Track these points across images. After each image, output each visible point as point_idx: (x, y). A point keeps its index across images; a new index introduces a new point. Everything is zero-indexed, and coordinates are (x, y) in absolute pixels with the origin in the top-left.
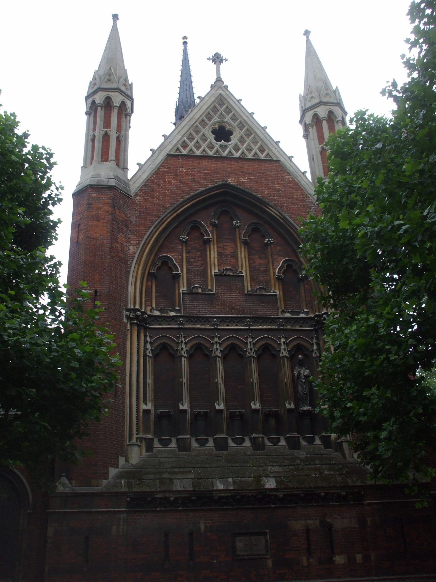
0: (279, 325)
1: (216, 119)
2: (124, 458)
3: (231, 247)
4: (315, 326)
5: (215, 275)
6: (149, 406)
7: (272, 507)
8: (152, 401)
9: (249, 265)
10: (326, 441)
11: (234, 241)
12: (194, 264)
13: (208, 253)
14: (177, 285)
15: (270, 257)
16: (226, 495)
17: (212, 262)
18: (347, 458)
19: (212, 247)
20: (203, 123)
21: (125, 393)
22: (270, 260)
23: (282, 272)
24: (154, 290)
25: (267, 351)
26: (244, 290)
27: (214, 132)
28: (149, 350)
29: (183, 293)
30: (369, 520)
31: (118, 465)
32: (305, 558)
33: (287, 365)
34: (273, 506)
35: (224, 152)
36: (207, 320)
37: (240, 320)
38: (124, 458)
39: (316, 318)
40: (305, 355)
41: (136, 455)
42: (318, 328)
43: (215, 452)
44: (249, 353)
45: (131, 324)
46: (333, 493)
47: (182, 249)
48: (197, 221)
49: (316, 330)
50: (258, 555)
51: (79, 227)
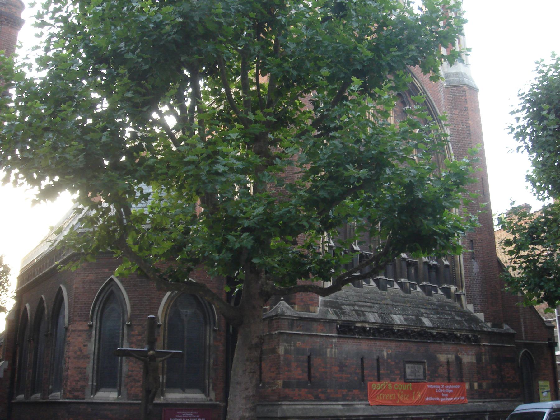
7: (428, 342)
10: (447, 292)
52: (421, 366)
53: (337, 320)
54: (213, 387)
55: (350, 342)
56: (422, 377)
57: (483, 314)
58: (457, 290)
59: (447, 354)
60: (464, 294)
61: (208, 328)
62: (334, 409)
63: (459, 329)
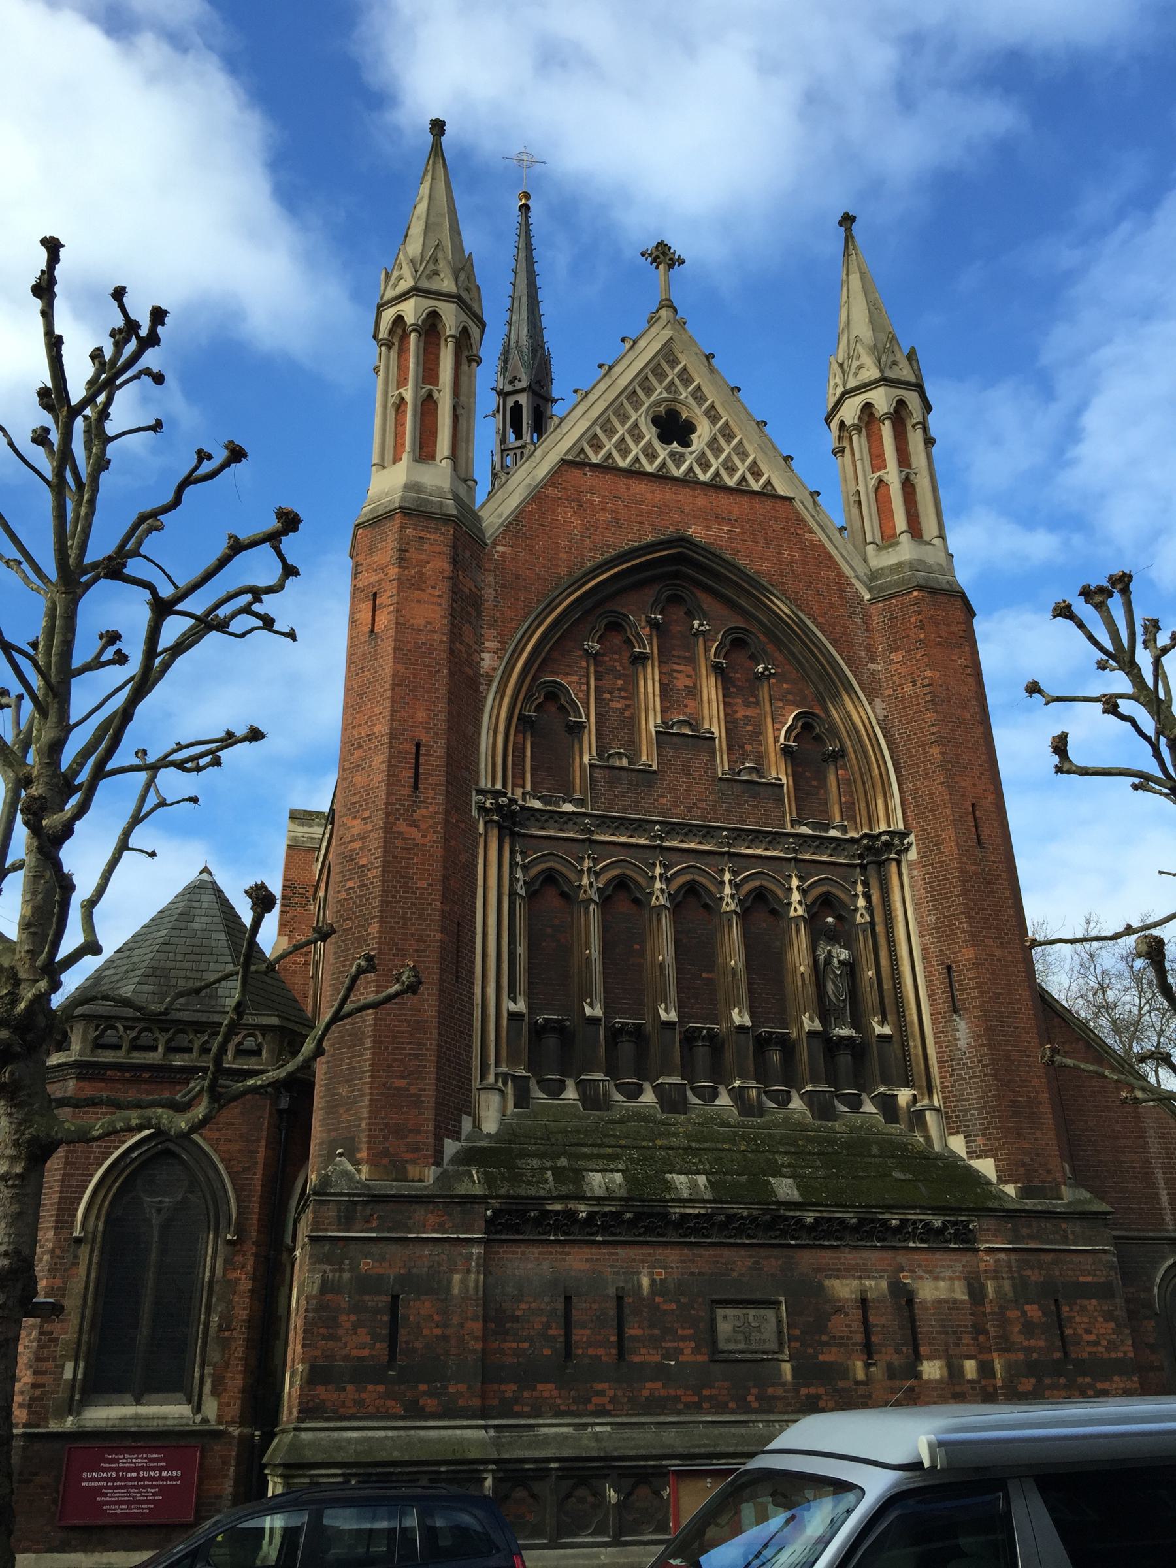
0: (787, 850)
1: (661, 393)
2: (471, 1118)
3: (688, 676)
4: (861, 857)
5: (657, 732)
6: (521, 1006)
9: (726, 715)
11: (692, 661)
12: (612, 704)
13: (642, 683)
14: (577, 747)
15: (767, 704)
16: (697, 1211)
17: (651, 706)
20: (632, 397)
21: (474, 973)
22: (768, 709)
23: (792, 739)
24: (528, 753)
26: (715, 769)
27: (656, 421)
28: (521, 883)
29: (591, 765)
30: (990, 1285)
32: (859, 1364)
34: (793, 1242)
35: (678, 468)
38: (471, 1118)
39: (865, 842)
40: (839, 918)
42: (868, 863)
43: (661, 1116)
44: (727, 904)
45: (486, 823)
46: (915, 1222)
47: (588, 669)
48: (616, 612)
49: (863, 867)
50: (764, 1353)
51: (374, 600)
52: (770, 1314)
53: (485, 1197)
54: (213, 1386)
55: (534, 1252)
56: (773, 1346)
57: (991, 1161)
58: (915, 1100)
59: (860, 1278)
60: (938, 1110)
61: (211, 1236)
62: (461, 1441)
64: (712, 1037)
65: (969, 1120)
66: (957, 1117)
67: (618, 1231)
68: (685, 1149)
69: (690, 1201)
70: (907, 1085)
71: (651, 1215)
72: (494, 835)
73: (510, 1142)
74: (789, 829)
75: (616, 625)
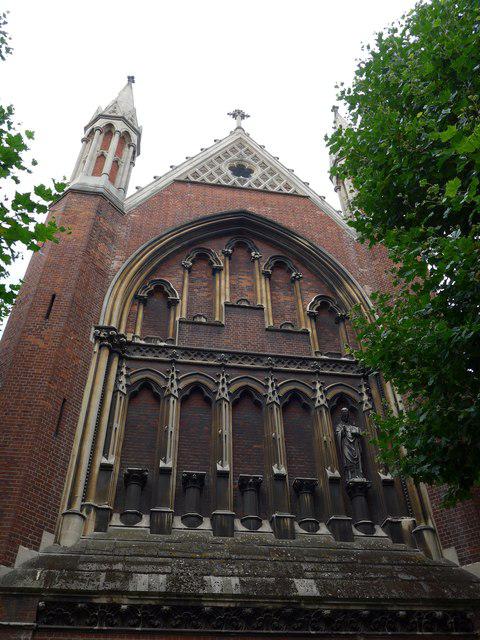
6: (111, 460)
8: (117, 454)
10: (395, 531)
11: (252, 275)
15: (299, 294)
16: (227, 605)
17: (223, 292)
18: (435, 558)
19: (223, 275)
25: (295, 401)
27: (231, 168)
31: (39, 545)
33: (326, 417)
36: (211, 354)
37: (258, 357)
41: (73, 533)
43: (211, 538)
46: (419, 614)
58: (415, 524)
60: (432, 531)
63: (402, 600)
64: (258, 484)
65: (457, 535)
66: (449, 534)
67: (157, 622)
68: (227, 559)
69: (221, 595)
70: (408, 515)
71: (186, 608)
72: (105, 353)
73: (81, 553)
74: (314, 356)
75: (203, 256)
